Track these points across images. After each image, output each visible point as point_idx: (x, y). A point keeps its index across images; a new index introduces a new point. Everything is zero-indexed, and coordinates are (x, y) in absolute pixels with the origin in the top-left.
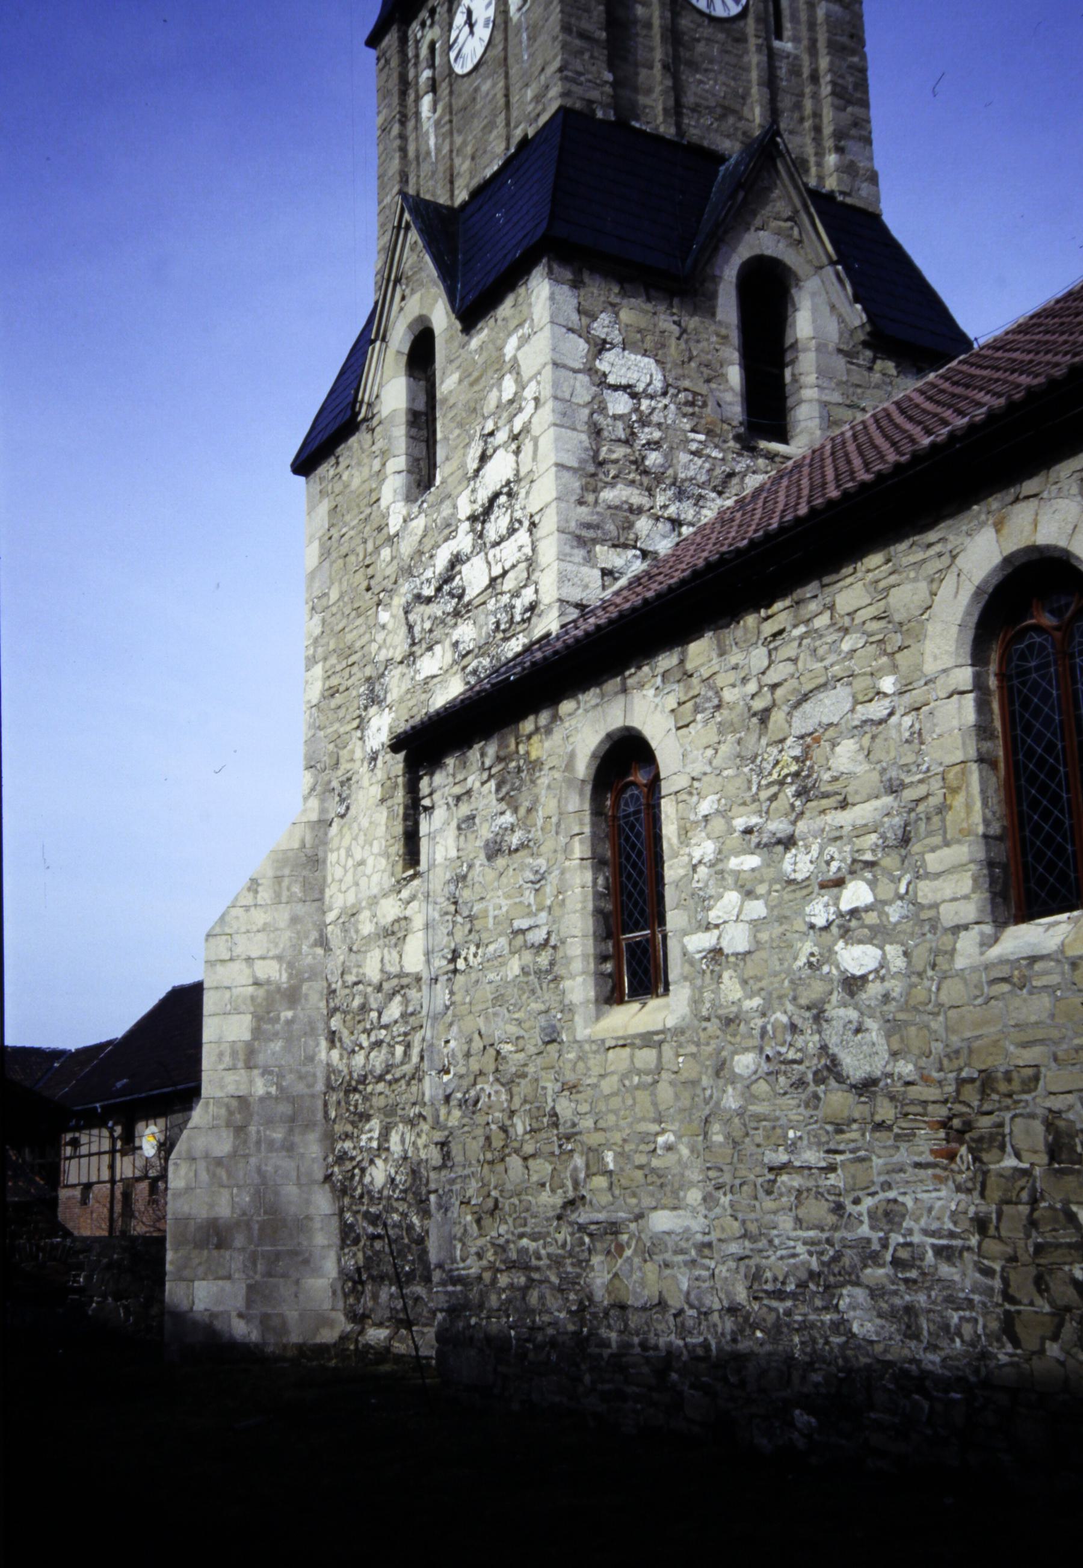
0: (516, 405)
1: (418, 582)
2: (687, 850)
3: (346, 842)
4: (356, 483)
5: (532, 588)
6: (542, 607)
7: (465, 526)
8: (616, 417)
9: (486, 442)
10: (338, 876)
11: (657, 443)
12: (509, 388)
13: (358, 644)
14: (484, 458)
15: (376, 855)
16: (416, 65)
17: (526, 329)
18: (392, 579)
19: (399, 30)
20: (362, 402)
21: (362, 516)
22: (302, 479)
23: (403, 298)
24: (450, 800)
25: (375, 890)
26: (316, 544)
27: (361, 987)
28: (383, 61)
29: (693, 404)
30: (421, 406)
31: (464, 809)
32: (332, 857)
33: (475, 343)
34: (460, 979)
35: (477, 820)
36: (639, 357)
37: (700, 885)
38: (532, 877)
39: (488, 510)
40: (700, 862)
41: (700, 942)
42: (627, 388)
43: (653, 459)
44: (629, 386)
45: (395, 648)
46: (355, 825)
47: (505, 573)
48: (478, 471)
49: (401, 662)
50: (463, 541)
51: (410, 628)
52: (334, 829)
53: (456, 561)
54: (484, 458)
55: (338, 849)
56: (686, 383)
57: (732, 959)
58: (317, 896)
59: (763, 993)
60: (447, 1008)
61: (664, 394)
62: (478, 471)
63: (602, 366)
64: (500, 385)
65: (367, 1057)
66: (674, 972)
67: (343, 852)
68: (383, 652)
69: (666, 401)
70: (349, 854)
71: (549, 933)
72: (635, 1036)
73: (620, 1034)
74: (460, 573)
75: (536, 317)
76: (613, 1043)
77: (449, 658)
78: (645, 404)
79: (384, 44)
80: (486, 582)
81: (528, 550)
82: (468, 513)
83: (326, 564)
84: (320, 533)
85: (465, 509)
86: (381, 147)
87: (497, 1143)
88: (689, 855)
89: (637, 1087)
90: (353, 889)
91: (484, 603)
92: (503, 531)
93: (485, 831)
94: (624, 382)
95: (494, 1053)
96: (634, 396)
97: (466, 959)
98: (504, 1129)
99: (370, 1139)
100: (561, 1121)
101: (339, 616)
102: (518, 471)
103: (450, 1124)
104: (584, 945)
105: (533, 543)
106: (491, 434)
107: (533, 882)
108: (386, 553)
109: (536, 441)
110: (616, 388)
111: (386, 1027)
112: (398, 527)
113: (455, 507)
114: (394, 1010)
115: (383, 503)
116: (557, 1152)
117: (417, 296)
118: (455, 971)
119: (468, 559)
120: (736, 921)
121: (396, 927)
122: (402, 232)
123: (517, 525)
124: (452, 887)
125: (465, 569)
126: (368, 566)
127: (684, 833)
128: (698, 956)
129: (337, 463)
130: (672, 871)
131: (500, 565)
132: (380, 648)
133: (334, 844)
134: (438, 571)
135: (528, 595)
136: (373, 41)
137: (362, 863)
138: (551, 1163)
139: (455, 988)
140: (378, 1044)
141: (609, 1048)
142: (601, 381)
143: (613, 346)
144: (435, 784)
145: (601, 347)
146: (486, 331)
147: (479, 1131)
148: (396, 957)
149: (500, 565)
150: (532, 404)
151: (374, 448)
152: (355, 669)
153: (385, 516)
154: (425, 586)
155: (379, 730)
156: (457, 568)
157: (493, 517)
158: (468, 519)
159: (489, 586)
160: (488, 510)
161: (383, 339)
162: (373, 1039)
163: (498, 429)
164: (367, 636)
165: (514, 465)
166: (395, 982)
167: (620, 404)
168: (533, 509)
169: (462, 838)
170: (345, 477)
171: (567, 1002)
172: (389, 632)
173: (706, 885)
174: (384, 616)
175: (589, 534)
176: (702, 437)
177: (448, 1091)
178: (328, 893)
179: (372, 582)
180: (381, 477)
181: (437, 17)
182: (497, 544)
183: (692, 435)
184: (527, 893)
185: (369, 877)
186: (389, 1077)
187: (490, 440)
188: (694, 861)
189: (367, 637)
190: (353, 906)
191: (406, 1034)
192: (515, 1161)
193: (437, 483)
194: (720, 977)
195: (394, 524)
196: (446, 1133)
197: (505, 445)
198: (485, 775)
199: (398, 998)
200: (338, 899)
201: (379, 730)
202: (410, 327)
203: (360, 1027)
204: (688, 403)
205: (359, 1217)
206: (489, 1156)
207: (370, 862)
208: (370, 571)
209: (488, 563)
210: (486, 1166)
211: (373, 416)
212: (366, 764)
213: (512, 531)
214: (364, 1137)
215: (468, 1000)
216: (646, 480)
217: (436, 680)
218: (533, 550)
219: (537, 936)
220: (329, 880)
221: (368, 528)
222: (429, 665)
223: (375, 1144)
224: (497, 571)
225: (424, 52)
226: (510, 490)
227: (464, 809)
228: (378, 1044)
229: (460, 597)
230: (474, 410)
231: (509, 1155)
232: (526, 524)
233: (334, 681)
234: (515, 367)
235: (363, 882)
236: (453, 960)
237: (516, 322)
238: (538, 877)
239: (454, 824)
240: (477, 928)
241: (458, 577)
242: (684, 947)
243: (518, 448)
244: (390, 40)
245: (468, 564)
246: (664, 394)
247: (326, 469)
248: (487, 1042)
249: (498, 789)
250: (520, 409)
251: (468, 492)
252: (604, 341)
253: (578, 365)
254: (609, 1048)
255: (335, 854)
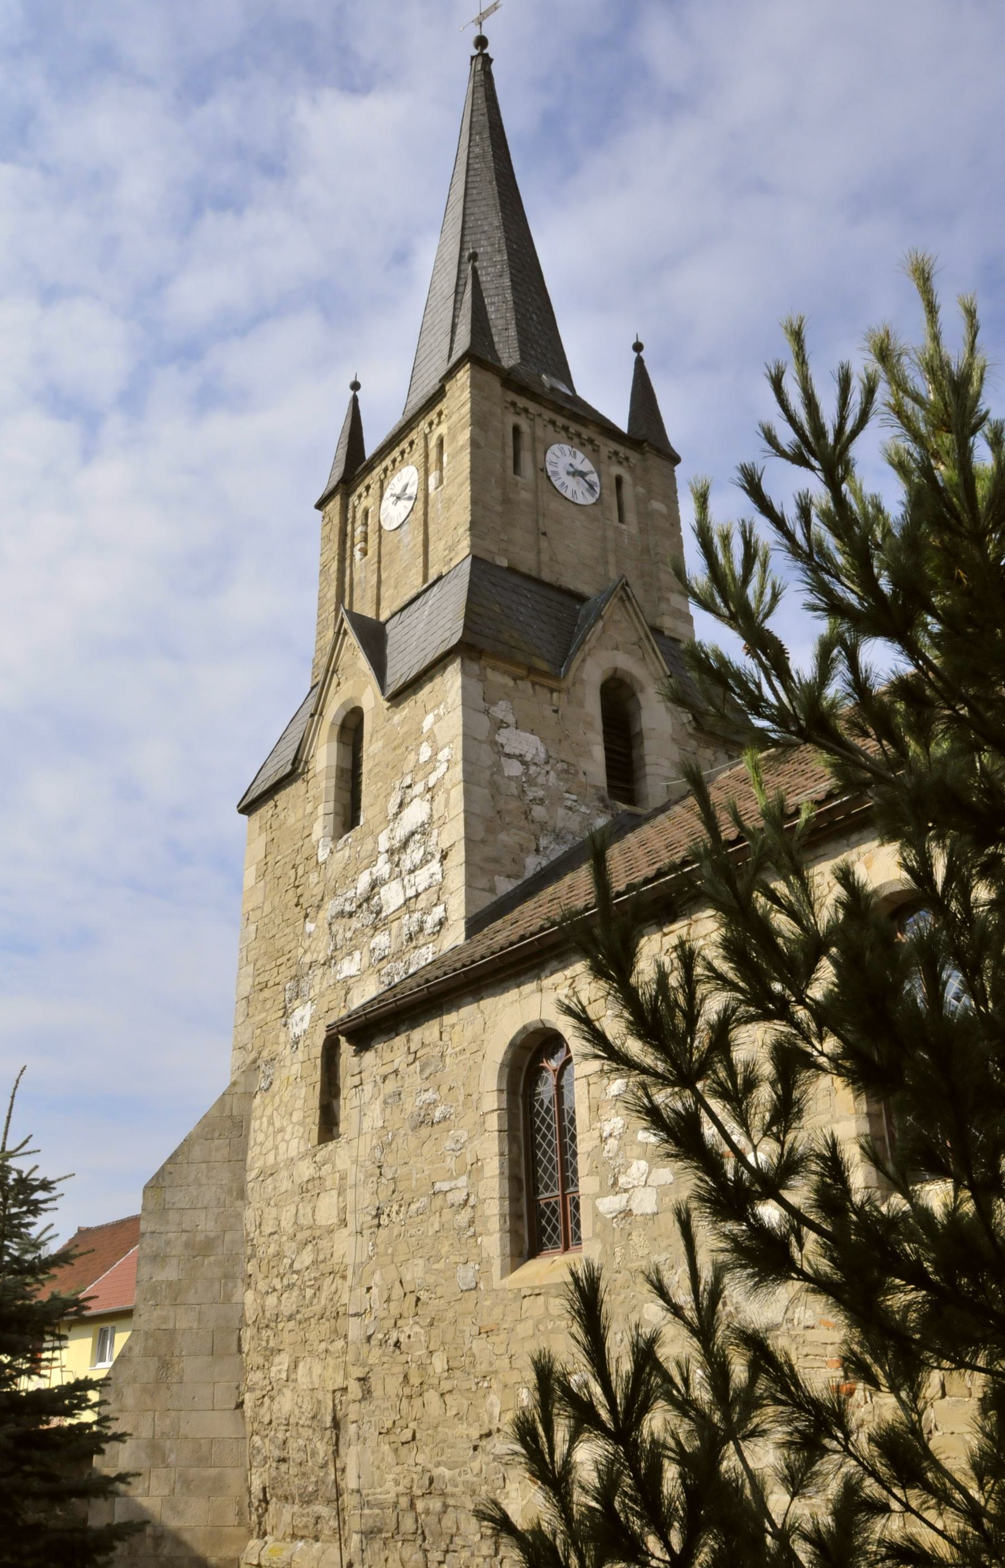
0: (431, 765)
1: (342, 899)
2: (599, 1125)
3: (268, 1112)
4: (291, 820)
5: (441, 907)
6: (450, 922)
7: (383, 858)
8: (510, 778)
9: (405, 793)
10: (259, 1141)
11: (541, 800)
12: (425, 752)
13: (287, 949)
14: (401, 805)
15: (294, 1124)
16: (353, 522)
17: (441, 710)
18: (319, 898)
19: (341, 499)
20: (301, 760)
21: (296, 847)
22: (245, 817)
23: (339, 684)
24: (378, 1078)
25: (293, 1153)
26: (254, 868)
27: (276, 1236)
28: (327, 520)
29: (569, 772)
30: (348, 765)
31: (391, 1086)
32: (255, 1124)
33: (397, 718)
34: (382, 1233)
35: (402, 1096)
36: (528, 734)
37: (610, 1155)
38: (453, 1146)
39: (405, 844)
40: (611, 1135)
41: (610, 1204)
42: (520, 757)
43: (539, 812)
44: (521, 755)
45: (319, 952)
46: (277, 1099)
47: (417, 895)
48: (397, 814)
49: (324, 964)
50: (382, 868)
51: (333, 936)
52: (257, 1101)
53: (375, 885)
54: (401, 805)
55: (261, 1117)
56: (563, 756)
57: (640, 1219)
58: (240, 1157)
59: (670, 1249)
60: (371, 1258)
61: (547, 763)
62: (397, 814)
63: (500, 739)
64: (419, 750)
65: (279, 1298)
66: (586, 1230)
67: (265, 1119)
68: (309, 955)
69: (548, 768)
70: (271, 1122)
71: (468, 1195)
72: (549, 1286)
73: (537, 1283)
74: (379, 894)
75: (450, 701)
76: (529, 1292)
77: (366, 961)
78: (533, 769)
79: (328, 508)
80: (402, 901)
81: (439, 877)
82: (387, 846)
83: (262, 883)
84: (257, 860)
85: (384, 844)
86: (323, 578)
87: (415, 1380)
88: (601, 1128)
89: (552, 1331)
90: (273, 1153)
91: (399, 918)
92: (417, 861)
93: (412, 1104)
94: (517, 752)
95: (414, 1299)
96: (524, 763)
97: (388, 1215)
98: (422, 1366)
99: (280, 1371)
100: (478, 1361)
101: (271, 925)
102: (431, 815)
103: (370, 1362)
104: (501, 1206)
105: (443, 871)
106: (409, 787)
107: (453, 1150)
108: (313, 878)
109: (448, 792)
110: (509, 756)
111: (297, 1272)
112: (326, 856)
113: (376, 842)
114: (306, 1258)
115: (314, 837)
116: (474, 1388)
117: (351, 682)
118: (379, 1225)
119: (386, 883)
120: (645, 1186)
121: (310, 1186)
122: (341, 636)
123: (429, 857)
124: (378, 1153)
125: (383, 890)
126: (298, 887)
127: (595, 1109)
128: (610, 1216)
129: (276, 806)
130: (585, 1143)
131: (414, 888)
132: (305, 952)
133: (257, 1113)
134: (359, 891)
135: (438, 912)
136: (321, 505)
137: (282, 1130)
138: (468, 1399)
139: (379, 1241)
140: (290, 1287)
141: (525, 1297)
142: (499, 749)
143: (508, 726)
144: (364, 1065)
145: (500, 725)
146: (407, 710)
147: (398, 1369)
148: (309, 1210)
149: (414, 888)
150: (445, 765)
151: (308, 795)
152: (282, 968)
153: (315, 847)
154: (347, 904)
155: (302, 1019)
156: (376, 890)
157: (409, 851)
158: (387, 851)
159: (405, 903)
160: (405, 844)
161: (321, 714)
162: (285, 1282)
163: (415, 783)
164: (295, 942)
165: (429, 811)
166: (308, 1233)
167: (514, 769)
168: (445, 845)
169: (388, 1110)
170: (282, 817)
171: (484, 1255)
172: (315, 939)
173: (617, 1155)
174: (310, 927)
175: (491, 866)
176: (574, 797)
177: (370, 1333)
178: (250, 1155)
179: (301, 900)
180: (313, 816)
181: (371, 491)
182: (411, 872)
183: (567, 795)
184: (448, 1159)
185: (288, 1142)
186: (298, 1317)
187: (409, 790)
188: (605, 1135)
189: (293, 944)
190: (273, 1166)
191: (315, 1279)
192: (432, 1396)
193: (361, 823)
194: (630, 1234)
195: (323, 855)
196: (367, 1369)
197: (421, 796)
198: (411, 1057)
199: (310, 1247)
200: (257, 1159)
201: (302, 1019)
202: (343, 705)
203: (275, 1271)
204: (567, 772)
205: (267, 1441)
206: (407, 1391)
207: (289, 1129)
208: (299, 891)
209: (404, 887)
210: (404, 1400)
211: (309, 770)
212: (288, 1047)
213: (425, 861)
214: (274, 1369)
215: (390, 1251)
216: (533, 827)
217: (353, 979)
218: (443, 878)
219: (459, 1197)
220: (252, 1143)
221: (299, 857)
222: (349, 967)
223: (284, 1376)
224: (411, 893)
225: (359, 514)
226: (423, 830)
227: (391, 1086)
228: (290, 1287)
229: (379, 913)
230: (395, 767)
231: (427, 1390)
232: (438, 856)
233: (262, 979)
234: (431, 737)
235: (282, 1147)
236: (378, 1216)
237: (432, 704)
238: (459, 1146)
239: (381, 1098)
240: (401, 1188)
241: (377, 897)
242: (595, 1208)
243: (432, 797)
244: (335, 505)
245: (386, 887)
246: (547, 763)
247: (266, 810)
248: (408, 1290)
249: (422, 1071)
250: (434, 769)
251: (386, 832)
252: (502, 721)
253: (482, 738)
254: (525, 1297)
255: (258, 1122)
